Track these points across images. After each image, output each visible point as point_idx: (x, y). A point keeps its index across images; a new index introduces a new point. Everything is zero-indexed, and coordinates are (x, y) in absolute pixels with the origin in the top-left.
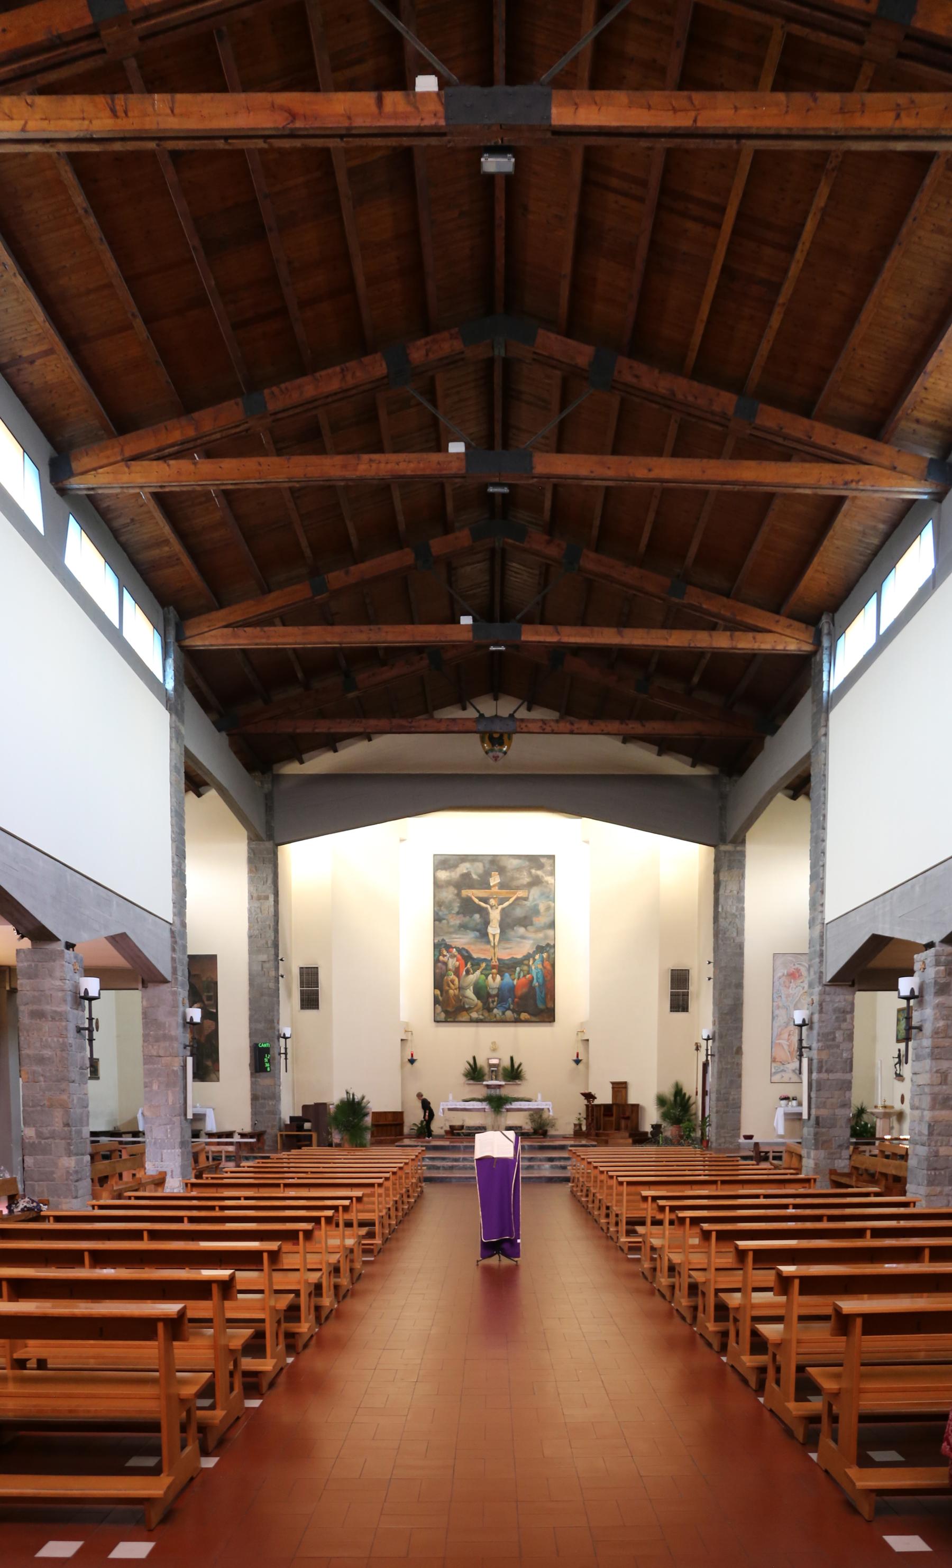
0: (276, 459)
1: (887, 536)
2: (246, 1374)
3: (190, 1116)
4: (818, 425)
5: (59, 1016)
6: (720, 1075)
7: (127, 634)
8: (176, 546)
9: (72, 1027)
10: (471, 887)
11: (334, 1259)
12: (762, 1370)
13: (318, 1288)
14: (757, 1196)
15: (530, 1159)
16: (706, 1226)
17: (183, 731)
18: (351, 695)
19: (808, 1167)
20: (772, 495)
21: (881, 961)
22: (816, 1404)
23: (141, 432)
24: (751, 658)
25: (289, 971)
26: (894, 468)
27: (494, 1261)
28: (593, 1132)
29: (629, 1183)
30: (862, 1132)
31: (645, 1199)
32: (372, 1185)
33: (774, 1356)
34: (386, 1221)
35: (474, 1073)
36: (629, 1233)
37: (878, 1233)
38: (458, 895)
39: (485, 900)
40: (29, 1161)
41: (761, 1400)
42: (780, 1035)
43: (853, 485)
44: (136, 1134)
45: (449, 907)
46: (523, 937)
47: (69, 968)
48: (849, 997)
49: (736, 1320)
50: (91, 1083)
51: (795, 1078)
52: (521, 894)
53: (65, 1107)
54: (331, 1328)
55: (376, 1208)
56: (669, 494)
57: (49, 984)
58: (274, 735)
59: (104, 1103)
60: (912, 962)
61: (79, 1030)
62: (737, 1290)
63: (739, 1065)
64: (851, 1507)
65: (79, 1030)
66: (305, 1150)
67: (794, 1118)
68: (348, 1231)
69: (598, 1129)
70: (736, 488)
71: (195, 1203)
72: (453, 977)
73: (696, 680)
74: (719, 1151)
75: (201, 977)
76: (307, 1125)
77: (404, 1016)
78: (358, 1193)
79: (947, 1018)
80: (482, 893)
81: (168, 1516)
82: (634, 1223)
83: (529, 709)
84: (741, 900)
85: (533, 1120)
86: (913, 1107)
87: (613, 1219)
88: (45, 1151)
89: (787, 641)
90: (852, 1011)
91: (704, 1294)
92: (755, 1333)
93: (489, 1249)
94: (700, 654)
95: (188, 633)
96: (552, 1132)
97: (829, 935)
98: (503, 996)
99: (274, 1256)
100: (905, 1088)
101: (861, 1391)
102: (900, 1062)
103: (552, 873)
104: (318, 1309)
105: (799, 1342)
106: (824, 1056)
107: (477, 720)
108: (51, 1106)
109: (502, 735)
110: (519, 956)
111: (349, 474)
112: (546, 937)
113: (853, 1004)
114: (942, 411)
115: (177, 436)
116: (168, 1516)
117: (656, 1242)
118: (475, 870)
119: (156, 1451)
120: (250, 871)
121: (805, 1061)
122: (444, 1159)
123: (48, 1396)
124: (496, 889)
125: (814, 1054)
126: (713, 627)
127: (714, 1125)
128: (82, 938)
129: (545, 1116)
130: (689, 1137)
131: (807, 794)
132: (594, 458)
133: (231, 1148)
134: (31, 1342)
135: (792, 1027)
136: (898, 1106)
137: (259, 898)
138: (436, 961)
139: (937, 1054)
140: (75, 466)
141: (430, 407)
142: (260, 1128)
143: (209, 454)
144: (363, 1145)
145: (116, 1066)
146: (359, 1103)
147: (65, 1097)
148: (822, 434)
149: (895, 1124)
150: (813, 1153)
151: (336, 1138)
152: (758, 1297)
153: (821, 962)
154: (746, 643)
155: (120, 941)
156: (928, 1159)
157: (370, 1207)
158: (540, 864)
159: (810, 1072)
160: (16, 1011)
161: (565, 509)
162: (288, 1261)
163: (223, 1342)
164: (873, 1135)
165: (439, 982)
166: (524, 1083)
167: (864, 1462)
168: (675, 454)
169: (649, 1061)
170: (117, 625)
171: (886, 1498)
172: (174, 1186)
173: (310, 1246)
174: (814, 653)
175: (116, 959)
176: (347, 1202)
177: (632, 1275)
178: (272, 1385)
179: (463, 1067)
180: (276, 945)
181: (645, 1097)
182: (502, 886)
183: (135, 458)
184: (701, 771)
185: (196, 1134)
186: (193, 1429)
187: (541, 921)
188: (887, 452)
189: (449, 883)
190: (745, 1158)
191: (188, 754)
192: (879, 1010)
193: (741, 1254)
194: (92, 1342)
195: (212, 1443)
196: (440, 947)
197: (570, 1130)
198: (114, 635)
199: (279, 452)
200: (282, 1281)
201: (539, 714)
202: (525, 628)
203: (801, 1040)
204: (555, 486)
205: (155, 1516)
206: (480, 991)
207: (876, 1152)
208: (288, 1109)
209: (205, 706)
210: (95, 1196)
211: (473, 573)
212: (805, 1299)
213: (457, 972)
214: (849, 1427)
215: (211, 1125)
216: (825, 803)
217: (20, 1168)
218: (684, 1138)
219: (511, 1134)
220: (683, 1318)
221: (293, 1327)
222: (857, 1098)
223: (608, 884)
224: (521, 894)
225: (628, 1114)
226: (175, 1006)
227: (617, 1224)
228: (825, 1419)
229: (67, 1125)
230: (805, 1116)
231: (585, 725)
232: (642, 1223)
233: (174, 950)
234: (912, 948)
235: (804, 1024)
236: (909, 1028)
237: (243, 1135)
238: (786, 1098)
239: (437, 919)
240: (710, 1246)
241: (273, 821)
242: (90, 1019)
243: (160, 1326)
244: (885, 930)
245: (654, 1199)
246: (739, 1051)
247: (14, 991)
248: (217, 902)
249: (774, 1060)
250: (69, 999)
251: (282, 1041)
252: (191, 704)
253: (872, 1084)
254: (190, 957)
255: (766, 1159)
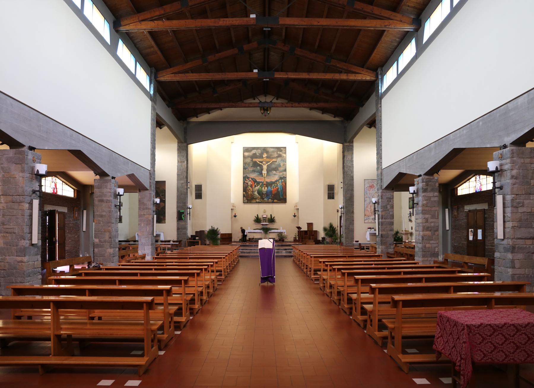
0: (191, 20)
1: (399, 43)
2: (175, 322)
3: (155, 235)
4: (375, 8)
5: (108, 201)
6: (346, 220)
7: (138, 76)
8: (156, 48)
9: (113, 205)
10: (256, 158)
11: (207, 283)
12: (365, 321)
13: (201, 293)
14: (361, 261)
15: (278, 249)
16: (343, 271)
17: (156, 107)
18: (215, 95)
19: (379, 251)
20: (360, 30)
21: (401, 182)
22: (385, 333)
23: (146, 12)
24: (354, 82)
25: (192, 186)
26: (401, 21)
27: (265, 284)
28: (301, 240)
29: (314, 257)
30: (398, 239)
31: (320, 262)
32: (221, 258)
33: (370, 316)
34: (226, 271)
35: (258, 220)
36: (314, 274)
37: (405, 273)
38: (252, 160)
39: (262, 162)
40: (96, 250)
41: (365, 331)
42: (367, 207)
43: (388, 27)
44: (135, 241)
45: (249, 164)
46: (275, 174)
47: (113, 185)
48: (392, 194)
49: (355, 304)
50: (119, 224)
51: (373, 221)
52: (274, 160)
53: (110, 232)
54: (206, 307)
55: (222, 266)
56: (325, 30)
57: (105, 190)
58: (187, 107)
59: (124, 231)
60: (414, 181)
61: (116, 206)
62: (356, 293)
63: (353, 217)
64: (400, 369)
65: (116, 206)
66: (196, 246)
67: (373, 235)
68: (212, 274)
69: (302, 239)
70: (348, 28)
71: (156, 264)
72: (250, 188)
73: (335, 89)
74: (346, 246)
75: (160, 188)
76: (197, 238)
77: (232, 201)
78: (216, 260)
79: (427, 200)
80: (260, 160)
81: (146, 372)
82: (316, 271)
83: (277, 99)
84: (352, 161)
85: (279, 236)
86: (416, 231)
87: (309, 269)
88: (102, 247)
89: (367, 76)
90: (393, 198)
91: (343, 295)
92: (363, 308)
93: (263, 280)
94: (336, 81)
95: (159, 76)
96: (286, 240)
97: (384, 172)
98: (268, 194)
99: (186, 281)
100: (413, 224)
101: (402, 327)
102: (410, 216)
103: (285, 153)
104: (201, 300)
105: (379, 311)
106: (383, 213)
107: (259, 103)
108: (105, 231)
109: (267, 108)
110: (274, 181)
111: (216, 25)
112: (283, 174)
113: (393, 196)
114: (417, 3)
115: (157, 13)
116: (146, 372)
117: (325, 277)
118: (258, 152)
119: (142, 349)
120: (178, 153)
121: (377, 215)
122: (247, 249)
123: (102, 329)
124: (265, 159)
125: (380, 213)
126: (341, 72)
127: (344, 237)
128: (118, 175)
129: (283, 235)
130: (335, 241)
131: (375, 127)
132: (300, 19)
133: (169, 246)
134: (96, 311)
135: (371, 204)
136: (410, 230)
137: (181, 162)
138: (244, 183)
139: (424, 212)
140: (122, 23)
141: (244, 3)
142: (180, 239)
143: (168, 19)
144: (217, 245)
145: (129, 218)
146: (216, 230)
147: (110, 228)
148: (377, 10)
149: (410, 237)
150: (380, 247)
151: (208, 242)
152: (363, 296)
153: (381, 182)
154: (352, 77)
155: (132, 176)
156: (422, 248)
157: (220, 265)
158: (281, 150)
159: (379, 219)
160: (93, 200)
161: (289, 35)
162: (191, 283)
163: (167, 311)
164: (402, 241)
165: (245, 189)
166: (275, 223)
167: (404, 353)
168: (327, 17)
169: (321, 216)
170: (134, 73)
171: (413, 365)
172: (148, 258)
173: (199, 278)
174: (376, 80)
175: (129, 182)
176: (212, 263)
177: (316, 289)
178: (184, 326)
179: (253, 218)
180: (187, 178)
181: (319, 227)
182: (267, 157)
183: (142, 21)
184: (337, 119)
185: (157, 241)
186: (156, 341)
187: (281, 169)
188: (399, 16)
189: (248, 156)
190: (356, 249)
191: (157, 115)
192: (402, 198)
193: (357, 281)
194: (118, 311)
195: (163, 346)
196: (245, 178)
197: (292, 240)
198: (133, 77)
199: (192, 18)
200: (188, 290)
201: (280, 101)
202: (276, 73)
203: (375, 208)
204: (286, 28)
205: (142, 371)
206: (260, 192)
207: (403, 246)
208: (190, 232)
209: (164, 99)
210: (120, 262)
211: (258, 56)
212: (380, 296)
213: (251, 186)
214: (398, 340)
215: (162, 238)
216: (381, 129)
217: (92, 253)
218: (334, 242)
219: (272, 240)
220: (336, 303)
221: (192, 306)
222: (396, 228)
223: (305, 157)
224: (274, 160)
225: (313, 234)
226: (150, 198)
227: (310, 271)
228: (389, 338)
229: (110, 238)
230: (377, 234)
231: (297, 104)
232: (320, 271)
233: (150, 179)
234: (414, 177)
235: (376, 203)
236: (413, 204)
237: (174, 242)
238: (370, 228)
239: (244, 168)
240: (345, 278)
241: (186, 137)
242: (120, 202)
243: (145, 305)
244: (404, 171)
245: (324, 262)
246: (353, 212)
247: (92, 193)
248: (166, 163)
249: (365, 215)
250: (113, 196)
251: (188, 210)
252: (159, 98)
253: (401, 223)
254: (156, 182)
255: (363, 249)
